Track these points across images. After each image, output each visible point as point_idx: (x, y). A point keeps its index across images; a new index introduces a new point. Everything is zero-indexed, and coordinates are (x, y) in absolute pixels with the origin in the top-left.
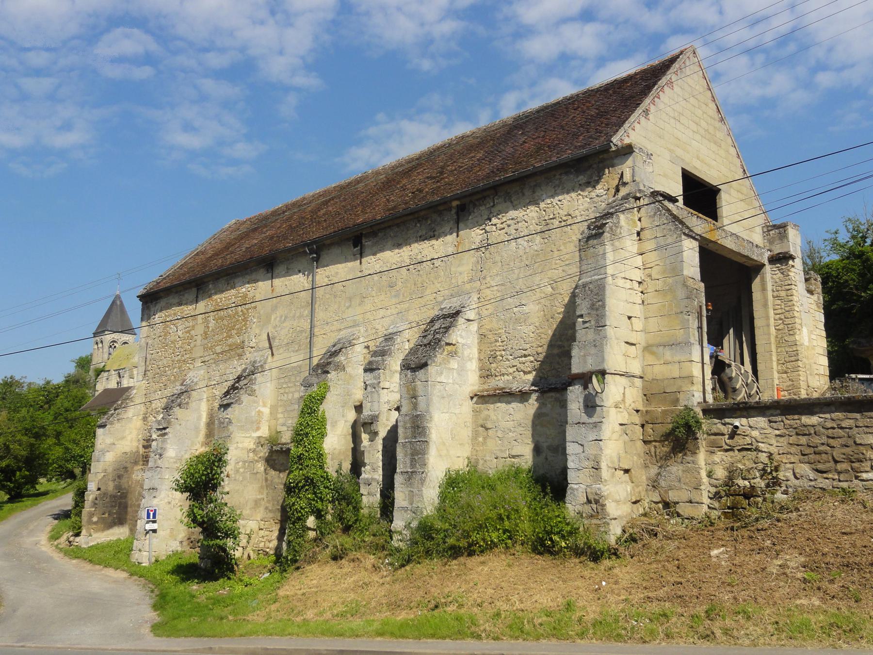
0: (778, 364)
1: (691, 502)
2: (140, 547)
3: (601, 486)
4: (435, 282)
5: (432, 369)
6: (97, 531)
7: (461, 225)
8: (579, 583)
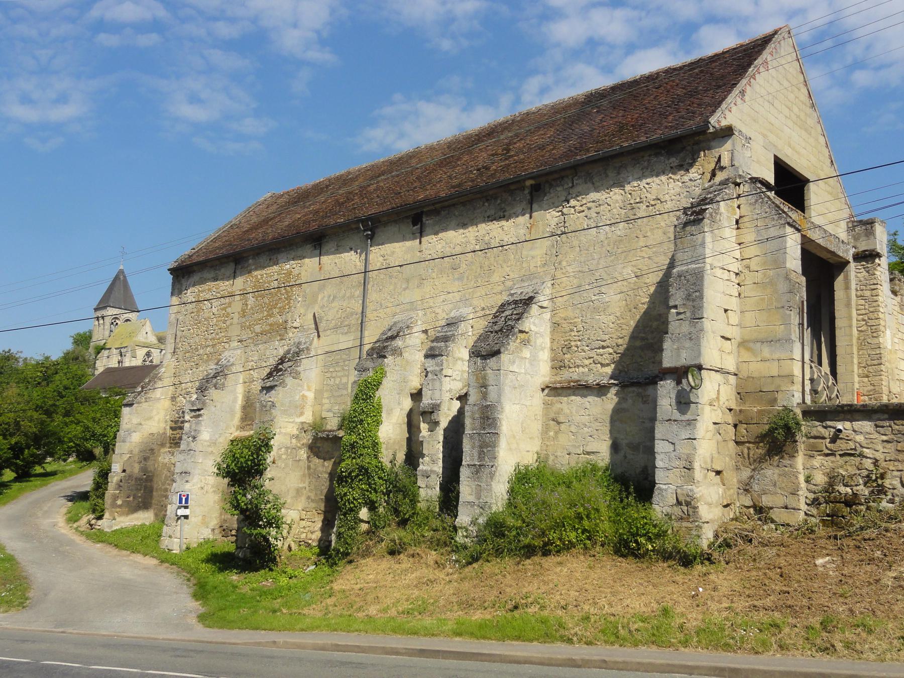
0: (859, 367)
1: (786, 508)
2: (170, 533)
3: (694, 487)
4: (505, 266)
5: (504, 357)
6: (121, 514)
7: (535, 206)
8: (672, 588)
